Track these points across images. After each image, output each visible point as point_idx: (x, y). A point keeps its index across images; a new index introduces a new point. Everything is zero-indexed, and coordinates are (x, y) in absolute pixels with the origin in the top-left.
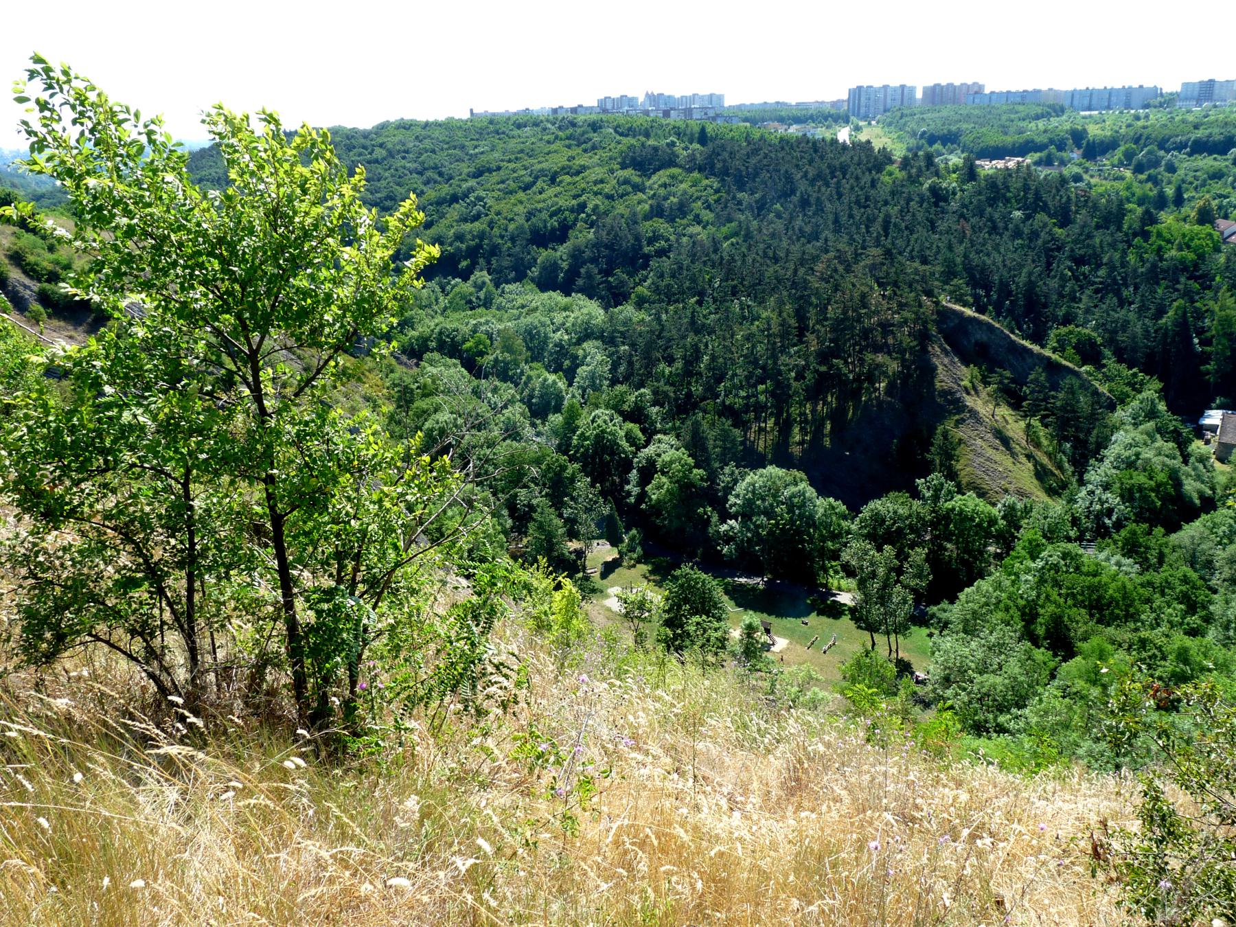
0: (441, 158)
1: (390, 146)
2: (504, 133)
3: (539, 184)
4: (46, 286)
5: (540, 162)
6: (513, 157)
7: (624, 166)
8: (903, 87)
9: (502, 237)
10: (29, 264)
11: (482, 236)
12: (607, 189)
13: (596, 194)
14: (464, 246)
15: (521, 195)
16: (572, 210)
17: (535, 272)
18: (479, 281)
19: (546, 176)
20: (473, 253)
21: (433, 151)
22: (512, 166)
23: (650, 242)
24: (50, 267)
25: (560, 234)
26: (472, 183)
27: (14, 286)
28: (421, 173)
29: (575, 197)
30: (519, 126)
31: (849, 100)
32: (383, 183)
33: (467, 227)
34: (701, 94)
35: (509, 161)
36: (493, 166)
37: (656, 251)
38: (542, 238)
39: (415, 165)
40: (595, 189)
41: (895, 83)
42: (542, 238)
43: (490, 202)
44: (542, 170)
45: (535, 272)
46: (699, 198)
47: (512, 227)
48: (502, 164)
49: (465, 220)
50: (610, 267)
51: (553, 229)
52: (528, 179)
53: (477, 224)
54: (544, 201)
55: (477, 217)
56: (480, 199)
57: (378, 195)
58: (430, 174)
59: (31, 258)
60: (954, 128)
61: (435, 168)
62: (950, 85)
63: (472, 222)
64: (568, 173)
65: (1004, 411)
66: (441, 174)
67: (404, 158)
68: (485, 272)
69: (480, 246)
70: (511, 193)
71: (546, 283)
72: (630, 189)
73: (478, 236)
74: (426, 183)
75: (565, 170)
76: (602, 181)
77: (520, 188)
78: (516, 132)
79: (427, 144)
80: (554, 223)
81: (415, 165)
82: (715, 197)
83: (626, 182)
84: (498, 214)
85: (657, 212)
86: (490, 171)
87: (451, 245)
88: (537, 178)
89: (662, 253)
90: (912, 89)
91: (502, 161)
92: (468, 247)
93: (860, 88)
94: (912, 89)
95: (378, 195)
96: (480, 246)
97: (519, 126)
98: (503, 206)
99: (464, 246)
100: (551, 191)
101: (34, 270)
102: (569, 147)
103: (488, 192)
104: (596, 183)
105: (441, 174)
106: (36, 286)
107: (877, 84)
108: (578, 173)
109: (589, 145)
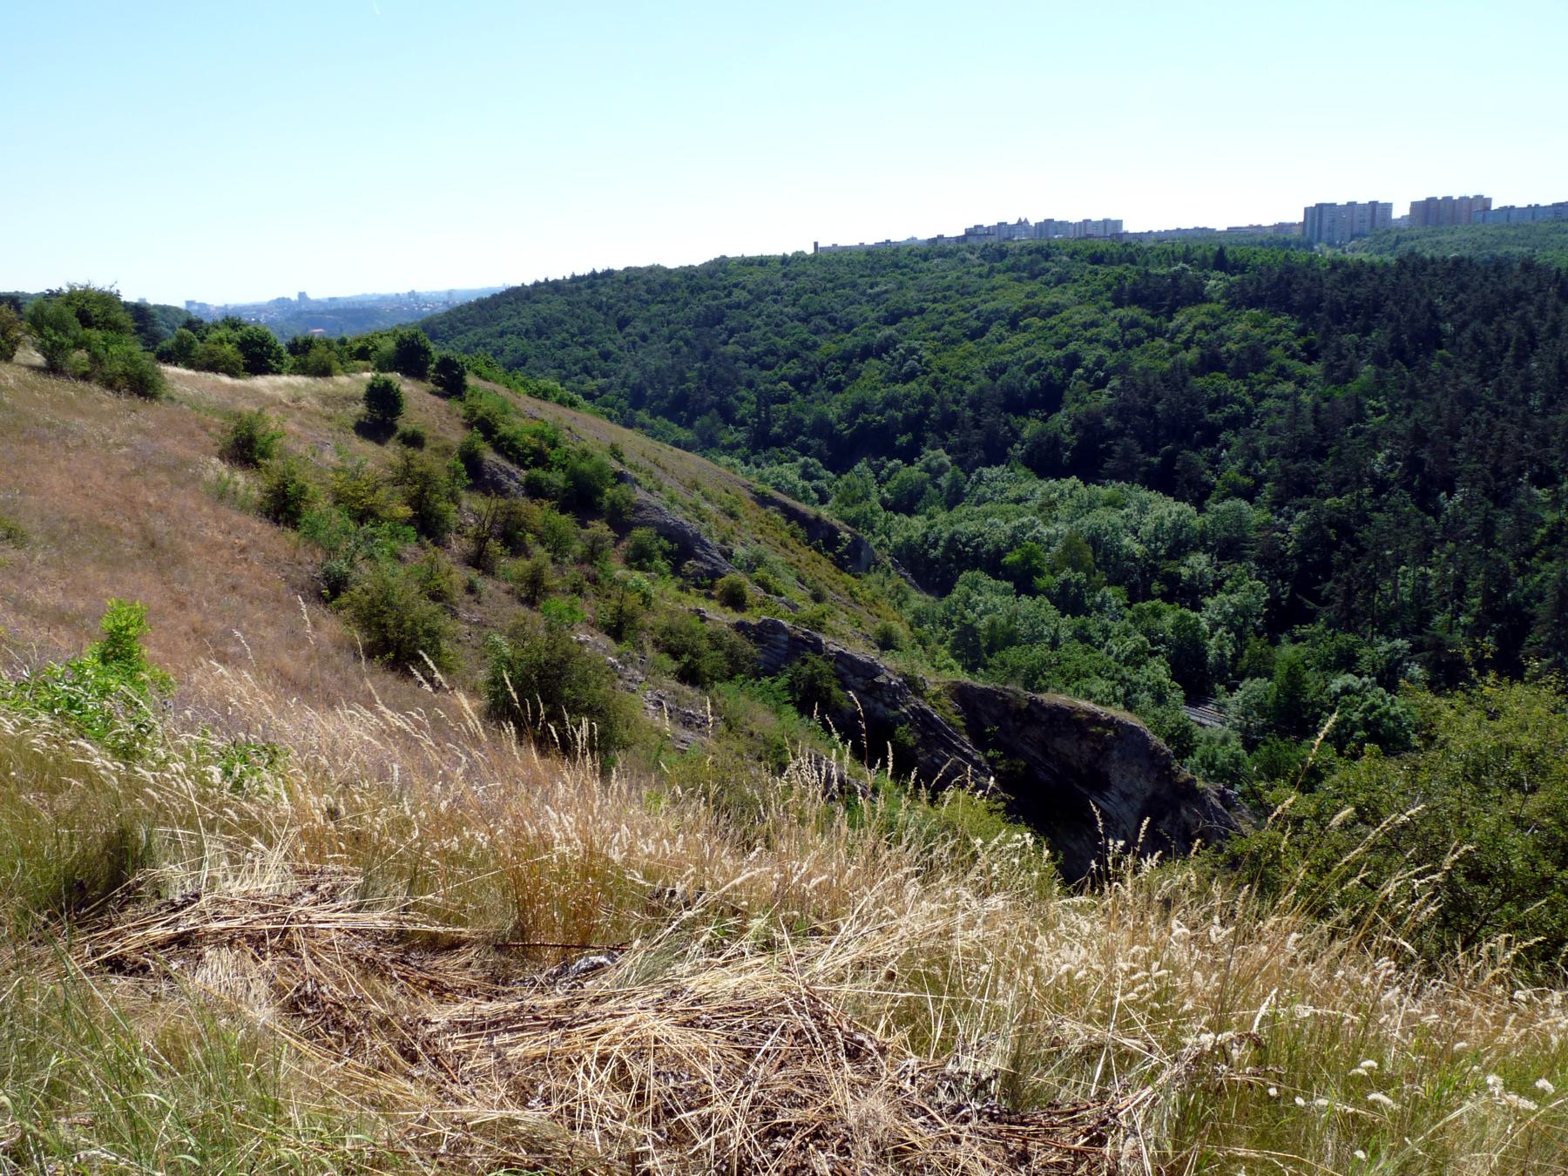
0: (826, 299)
1: (751, 286)
2: (906, 266)
3: (996, 329)
4: (538, 472)
5: (985, 302)
6: (939, 295)
7: (1119, 303)
8: (1374, 204)
9: (956, 402)
10: (504, 438)
11: (926, 400)
12: (1106, 333)
13: (1090, 341)
14: (900, 415)
15: (969, 345)
16: (1057, 364)
17: (1018, 450)
18: (934, 464)
19: (1003, 318)
20: (915, 424)
21: (814, 292)
22: (940, 307)
23: (1214, 405)
24: (535, 443)
25: (1049, 398)
26: (888, 331)
27: (494, 474)
28: (805, 320)
29: (1060, 346)
30: (926, 258)
31: (1303, 224)
32: (754, 333)
33: (900, 389)
34: (1094, 219)
35: (935, 301)
36: (914, 307)
37: (1226, 420)
38: (1017, 404)
39: (796, 310)
40: (1088, 334)
41: (1363, 199)
42: (1017, 404)
43: (927, 355)
44: (996, 311)
45: (1018, 450)
46: (1276, 343)
47: (970, 389)
48: (925, 305)
49: (895, 380)
50: (1159, 441)
51: (1034, 392)
52: (975, 324)
53: (913, 385)
54: (1012, 352)
55: (910, 376)
56: (912, 351)
57: (754, 349)
58: (817, 320)
59: (504, 429)
60: (1500, 253)
61: (823, 313)
62: (1447, 199)
63: (905, 382)
64: (1035, 315)
65: (638, 575)
66: (832, 321)
67: (775, 301)
68: (941, 451)
69: (924, 415)
70: (954, 342)
71: (1045, 462)
72: (1144, 334)
73: (919, 403)
74: (816, 332)
75: (1027, 310)
76: (1094, 324)
77: (965, 335)
78: (924, 265)
79: (803, 282)
80: (1033, 381)
81: (796, 310)
82: (1302, 341)
83: (1134, 323)
84: (943, 370)
85: (1211, 363)
86: (910, 314)
87: (880, 413)
88: (989, 322)
89: (1234, 423)
90: (1387, 207)
91: (925, 300)
92: (906, 417)
93: (1320, 206)
94: (1387, 207)
95: (754, 349)
96: (924, 415)
97: (926, 258)
98: (946, 359)
99: (900, 415)
100: (1018, 339)
101: (512, 447)
102: (1019, 280)
103: (915, 337)
104: (1086, 326)
105: (832, 321)
106: (523, 475)
107: (1341, 201)
108: (1050, 314)
109: (1048, 277)
